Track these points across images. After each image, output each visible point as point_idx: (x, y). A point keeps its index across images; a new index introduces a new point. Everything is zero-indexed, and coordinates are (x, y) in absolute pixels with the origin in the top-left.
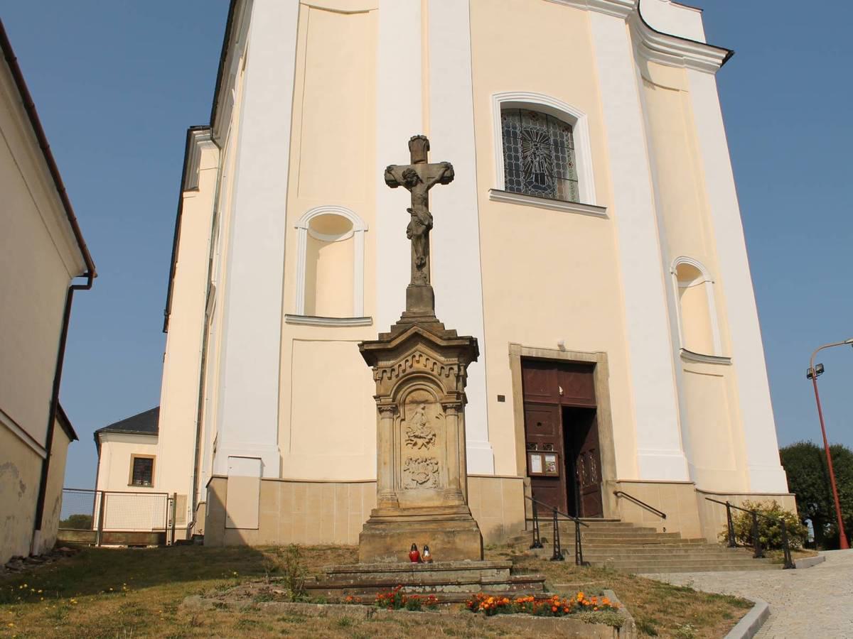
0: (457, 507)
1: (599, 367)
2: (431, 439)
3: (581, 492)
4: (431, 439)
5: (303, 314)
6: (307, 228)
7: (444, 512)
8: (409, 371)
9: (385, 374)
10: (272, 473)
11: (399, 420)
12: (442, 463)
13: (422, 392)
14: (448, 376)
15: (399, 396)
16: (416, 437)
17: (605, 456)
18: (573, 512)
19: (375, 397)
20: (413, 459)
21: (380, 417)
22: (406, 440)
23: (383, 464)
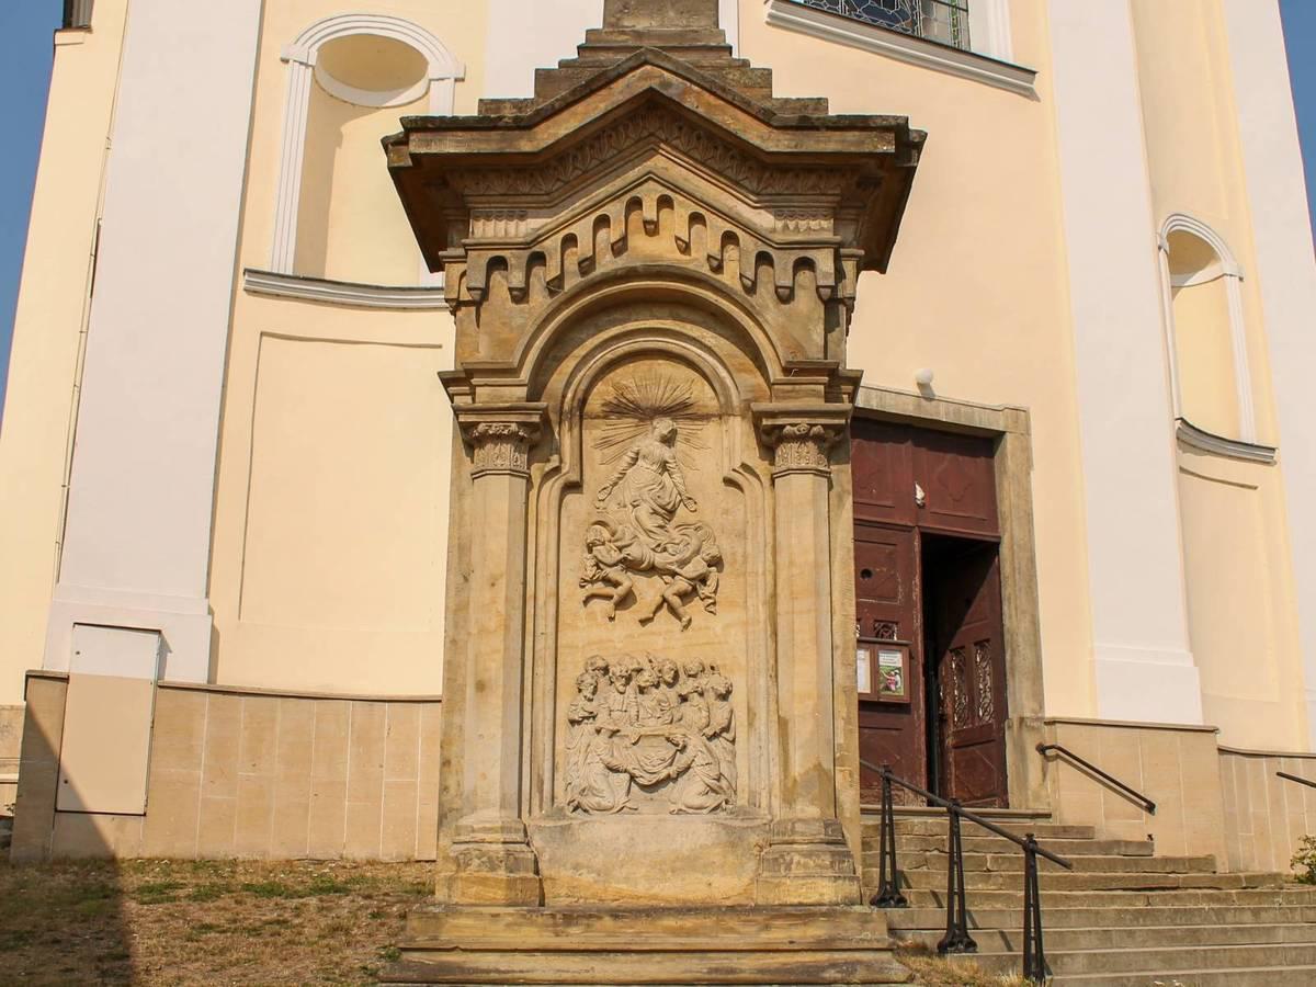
0: (830, 912)
1: (1009, 443)
2: (703, 580)
3: (949, 741)
4: (703, 580)
5: (289, 272)
6: (312, 62)
7: (765, 937)
8: (607, 264)
9: (497, 276)
10: (188, 667)
11: (553, 487)
12: (751, 692)
13: (664, 367)
14: (785, 296)
15: (557, 381)
16: (630, 565)
17: (1017, 660)
18: (935, 786)
19: (448, 381)
20: (615, 670)
21: (468, 467)
22: (584, 582)
23: (470, 690)
